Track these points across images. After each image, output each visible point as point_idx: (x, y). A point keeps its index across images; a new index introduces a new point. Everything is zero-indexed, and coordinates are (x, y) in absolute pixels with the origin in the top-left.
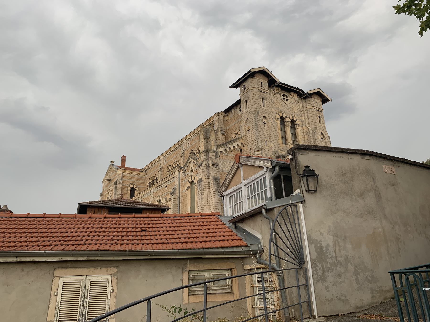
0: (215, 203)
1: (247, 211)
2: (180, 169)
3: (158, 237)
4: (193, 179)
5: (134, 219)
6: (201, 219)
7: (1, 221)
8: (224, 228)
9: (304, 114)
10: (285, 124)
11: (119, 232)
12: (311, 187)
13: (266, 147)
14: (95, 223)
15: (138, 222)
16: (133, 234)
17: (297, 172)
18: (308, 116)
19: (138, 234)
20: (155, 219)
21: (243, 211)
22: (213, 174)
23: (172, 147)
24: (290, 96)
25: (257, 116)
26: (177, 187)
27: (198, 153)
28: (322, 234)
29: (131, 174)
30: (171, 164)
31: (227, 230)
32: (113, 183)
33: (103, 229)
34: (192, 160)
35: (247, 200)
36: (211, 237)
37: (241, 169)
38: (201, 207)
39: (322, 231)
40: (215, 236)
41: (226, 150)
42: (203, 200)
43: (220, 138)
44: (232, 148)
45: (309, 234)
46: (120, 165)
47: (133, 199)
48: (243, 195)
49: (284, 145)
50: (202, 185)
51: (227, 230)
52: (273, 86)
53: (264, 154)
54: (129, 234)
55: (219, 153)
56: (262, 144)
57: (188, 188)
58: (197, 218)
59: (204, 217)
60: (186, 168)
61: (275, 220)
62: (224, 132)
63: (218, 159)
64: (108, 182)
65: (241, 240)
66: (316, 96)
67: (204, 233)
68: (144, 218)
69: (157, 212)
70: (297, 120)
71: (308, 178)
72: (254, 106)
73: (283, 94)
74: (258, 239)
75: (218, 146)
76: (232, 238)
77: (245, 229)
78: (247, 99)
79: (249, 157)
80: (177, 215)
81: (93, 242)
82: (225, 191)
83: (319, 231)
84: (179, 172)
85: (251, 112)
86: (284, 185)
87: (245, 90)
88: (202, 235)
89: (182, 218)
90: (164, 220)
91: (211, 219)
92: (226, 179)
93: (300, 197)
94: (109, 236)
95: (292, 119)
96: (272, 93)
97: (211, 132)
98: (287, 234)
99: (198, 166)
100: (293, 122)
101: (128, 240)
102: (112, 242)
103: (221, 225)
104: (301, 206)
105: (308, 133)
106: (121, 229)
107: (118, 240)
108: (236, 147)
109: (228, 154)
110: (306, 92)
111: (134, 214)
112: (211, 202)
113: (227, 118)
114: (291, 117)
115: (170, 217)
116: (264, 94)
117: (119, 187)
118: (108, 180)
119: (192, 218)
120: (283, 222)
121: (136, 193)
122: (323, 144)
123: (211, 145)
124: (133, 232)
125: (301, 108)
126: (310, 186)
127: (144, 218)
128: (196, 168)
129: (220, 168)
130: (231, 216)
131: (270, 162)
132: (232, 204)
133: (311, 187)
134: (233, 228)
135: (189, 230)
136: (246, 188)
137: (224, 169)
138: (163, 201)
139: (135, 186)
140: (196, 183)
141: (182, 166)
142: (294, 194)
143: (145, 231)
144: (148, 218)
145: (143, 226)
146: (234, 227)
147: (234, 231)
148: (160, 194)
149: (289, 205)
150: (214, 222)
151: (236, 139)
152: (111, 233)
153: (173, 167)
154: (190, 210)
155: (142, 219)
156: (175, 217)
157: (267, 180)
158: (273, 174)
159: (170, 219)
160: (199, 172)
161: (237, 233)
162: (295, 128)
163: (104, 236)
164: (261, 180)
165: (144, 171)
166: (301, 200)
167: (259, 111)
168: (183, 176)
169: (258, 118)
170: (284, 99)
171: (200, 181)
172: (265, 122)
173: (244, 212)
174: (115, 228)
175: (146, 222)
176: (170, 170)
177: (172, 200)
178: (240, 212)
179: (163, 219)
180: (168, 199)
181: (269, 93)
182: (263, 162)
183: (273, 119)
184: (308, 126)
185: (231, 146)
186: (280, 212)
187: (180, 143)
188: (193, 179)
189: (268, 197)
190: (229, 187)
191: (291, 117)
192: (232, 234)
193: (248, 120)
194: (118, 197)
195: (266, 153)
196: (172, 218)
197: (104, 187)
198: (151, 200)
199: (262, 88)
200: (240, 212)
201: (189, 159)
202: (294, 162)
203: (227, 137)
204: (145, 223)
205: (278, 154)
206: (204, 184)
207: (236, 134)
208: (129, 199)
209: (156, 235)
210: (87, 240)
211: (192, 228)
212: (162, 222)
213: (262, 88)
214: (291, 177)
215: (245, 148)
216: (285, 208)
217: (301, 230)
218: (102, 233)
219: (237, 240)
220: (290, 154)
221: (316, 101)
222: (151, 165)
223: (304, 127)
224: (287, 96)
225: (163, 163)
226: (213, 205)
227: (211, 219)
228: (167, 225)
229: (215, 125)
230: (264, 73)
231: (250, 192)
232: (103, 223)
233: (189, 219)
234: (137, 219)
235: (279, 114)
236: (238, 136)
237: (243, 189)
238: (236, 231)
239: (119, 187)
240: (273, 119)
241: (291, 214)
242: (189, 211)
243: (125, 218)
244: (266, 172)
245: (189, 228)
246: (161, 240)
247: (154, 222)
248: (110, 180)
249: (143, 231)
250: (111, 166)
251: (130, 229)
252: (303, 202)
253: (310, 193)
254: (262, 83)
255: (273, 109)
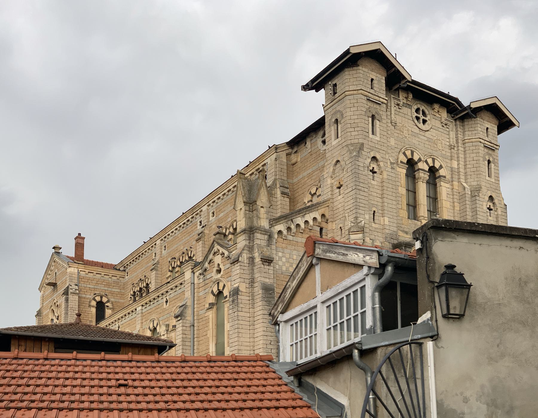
0: (265, 338)
1: (323, 354)
2: (195, 266)
3: (151, 398)
4: (221, 288)
5: (104, 363)
6: (234, 367)
7: (2, 364)
8: (279, 385)
9: (458, 154)
10: (417, 176)
11: (74, 386)
12: (455, 308)
13: (373, 225)
14: (26, 368)
15: (112, 369)
16: (101, 391)
17: (428, 277)
18: (465, 158)
19: (111, 391)
20: (145, 364)
21: (316, 353)
22: (263, 279)
23: (177, 220)
24: (432, 112)
25: (358, 156)
26: (189, 303)
27: (233, 234)
28: (466, 400)
29: (95, 275)
30: (177, 256)
31: (284, 388)
32: (61, 291)
33: (43, 381)
34: (219, 247)
35: (325, 332)
36: (254, 400)
37: (318, 269)
38: (236, 344)
39: (468, 394)
40: (261, 400)
41: (289, 229)
42: (240, 330)
43: (279, 203)
44: (303, 226)
45: (442, 400)
46: (72, 253)
47: (103, 324)
48: (318, 322)
49: (410, 221)
50: (240, 301)
51: (284, 388)
52: (397, 90)
53: (367, 240)
54: (75, 390)
55: (276, 236)
56: (365, 218)
57: (211, 305)
58: (226, 364)
59: (240, 364)
60: (206, 265)
61: (375, 370)
62: (287, 191)
63: (274, 247)
64: (50, 288)
65: (309, 407)
66: (486, 115)
67: (239, 393)
68: (123, 361)
69: (149, 351)
70: (441, 167)
71: (450, 289)
72: (353, 134)
73: (416, 107)
74: (341, 407)
75: (274, 219)
76: (293, 403)
77: (319, 387)
78: (338, 116)
79: (334, 244)
80: (187, 359)
81: (24, 404)
82: (283, 313)
83: (462, 394)
84: (193, 272)
85: (347, 146)
86: (401, 303)
87: (337, 95)
88: (236, 396)
89: (197, 364)
90: (162, 367)
91: (254, 367)
92: (285, 289)
93: (431, 328)
94: (55, 394)
95: (431, 165)
96: (393, 105)
97: (259, 190)
98: (398, 398)
99: (231, 261)
100: (433, 170)
101: (92, 402)
102: (61, 405)
103: (274, 379)
104: (429, 345)
105: (462, 197)
106: (78, 382)
107: (73, 402)
108: (311, 223)
109: (295, 239)
110: (465, 104)
111: (103, 353)
112: (256, 335)
113: (294, 158)
114: (430, 161)
115: (173, 362)
116: (376, 106)
117: (73, 299)
118: (49, 284)
119: (217, 364)
120: (392, 377)
121: (108, 312)
122: (492, 221)
123: (258, 218)
124: (101, 387)
125: (453, 141)
126: (452, 305)
127: (123, 361)
128: (228, 265)
129: (277, 267)
130: (292, 363)
131: (375, 256)
132: (297, 339)
133: (455, 308)
134: (294, 386)
135: (210, 387)
136: (325, 308)
137: (284, 268)
138: (161, 330)
139: (105, 300)
140: (226, 297)
141: (200, 259)
142: (420, 321)
143: (125, 386)
144: (130, 361)
145: (120, 376)
146: (296, 384)
147: (297, 390)
148: (154, 316)
149: (406, 343)
150: (261, 373)
151: (313, 205)
152: (59, 388)
153: (181, 263)
154: (214, 350)
155: (119, 363)
156: (185, 361)
157: (369, 292)
158: (381, 281)
159: (174, 364)
160: (233, 274)
161: (302, 394)
162: (435, 185)
163: (45, 394)
164: (355, 292)
165: (122, 269)
166: (430, 334)
167: (363, 144)
168: (201, 280)
169: (360, 159)
170: (418, 118)
171: (236, 292)
172: (375, 170)
173: (319, 355)
174: (49, 378)
175: (127, 369)
176: (173, 268)
177: (179, 329)
178: (311, 354)
179: (160, 365)
180: (171, 327)
181: (387, 104)
182: (361, 255)
183: (391, 163)
184: (462, 180)
185: (300, 220)
186: (387, 355)
187: (195, 210)
188: (221, 288)
189: (368, 326)
190: (291, 306)
191: (430, 161)
192: (292, 395)
193: (338, 165)
194: (72, 319)
195: (372, 237)
196: (178, 364)
197: (43, 299)
198: (138, 327)
199: (372, 91)
200: (311, 354)
201: (212, 246)
202: (425, 255)
203: (293, 201)
204: (124, 370)
205: (397, 239)
206: (243, 298)
207: (312, 195)
208: (94, 324)
209: (146, 395)
210: (12, 401)
211: (217, 383)
212: (158, 369)
213: (372, 91)
214: (415, 287)
215: (330, 226)
216: (399, 348)
217: (426, 392)
218: (41, 387)
219: (301, 407)
220: (417, 239)
221: (486, 125)
222: (136, 256)
223: (456, 183)
224: (424, 114)
225: (161, 253)
226: (261, 342)
227: (254, 367)
228: (168, 376)
229: (268, 173)
230: (378, 57)
231: (332, 314)
232: (43, 368)
233: (212, 367)
234: (109, 364)
235: (404, 154)
236: (315, 200)
237: (318, 310)
238: (301, 391)
239: (73, 299)
240: (391, 163)
241: (409, 361)
242: (212, 351)
243: (85, 360)
244: (367, 275)
245: (210, 383)
246: (157, 405)
247: (143, 370)
248: (54, 285)
249: (120, 385)
250: (55, 256)
251: (96, 382)
252: (435, 337)
253: (451, 320)
254: (372, 80)
255: (392, 142)
